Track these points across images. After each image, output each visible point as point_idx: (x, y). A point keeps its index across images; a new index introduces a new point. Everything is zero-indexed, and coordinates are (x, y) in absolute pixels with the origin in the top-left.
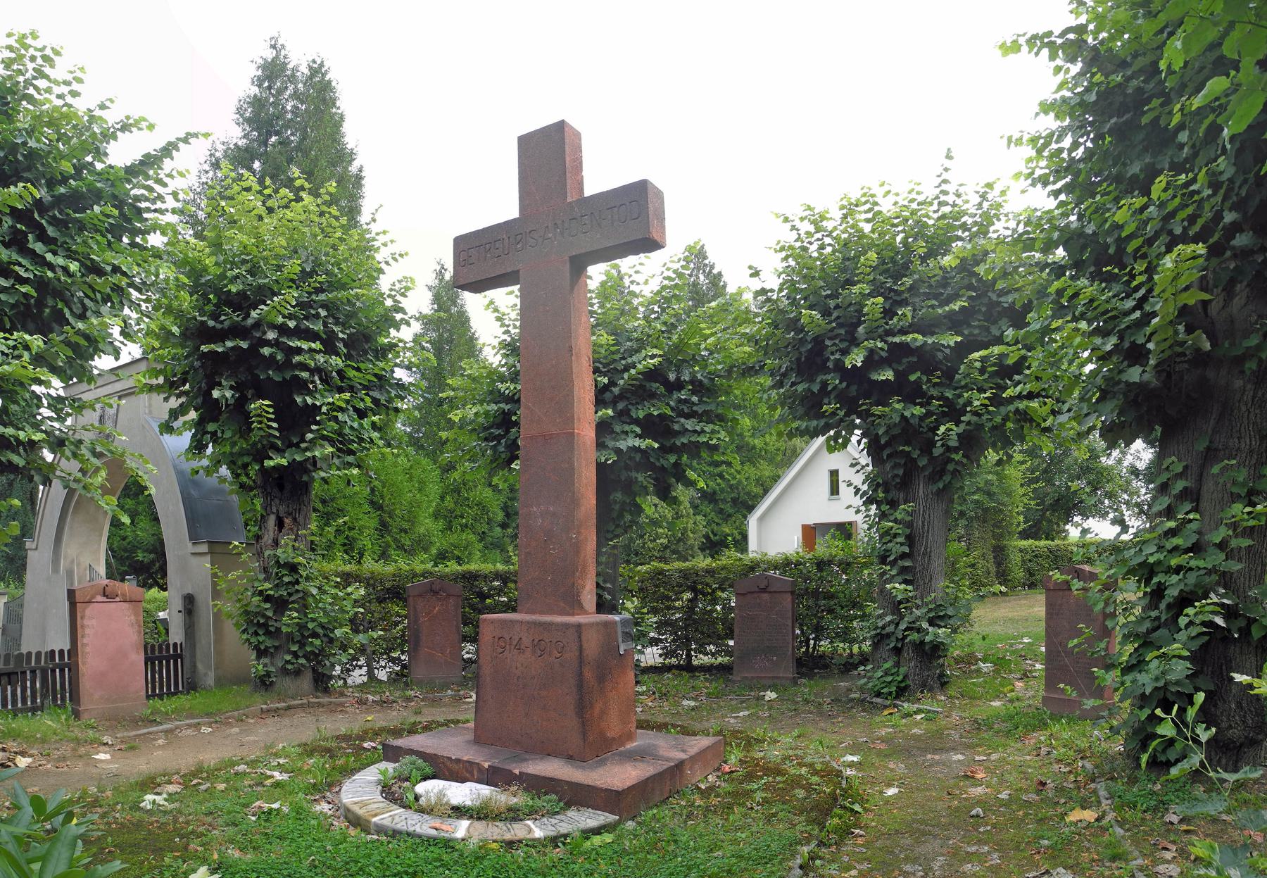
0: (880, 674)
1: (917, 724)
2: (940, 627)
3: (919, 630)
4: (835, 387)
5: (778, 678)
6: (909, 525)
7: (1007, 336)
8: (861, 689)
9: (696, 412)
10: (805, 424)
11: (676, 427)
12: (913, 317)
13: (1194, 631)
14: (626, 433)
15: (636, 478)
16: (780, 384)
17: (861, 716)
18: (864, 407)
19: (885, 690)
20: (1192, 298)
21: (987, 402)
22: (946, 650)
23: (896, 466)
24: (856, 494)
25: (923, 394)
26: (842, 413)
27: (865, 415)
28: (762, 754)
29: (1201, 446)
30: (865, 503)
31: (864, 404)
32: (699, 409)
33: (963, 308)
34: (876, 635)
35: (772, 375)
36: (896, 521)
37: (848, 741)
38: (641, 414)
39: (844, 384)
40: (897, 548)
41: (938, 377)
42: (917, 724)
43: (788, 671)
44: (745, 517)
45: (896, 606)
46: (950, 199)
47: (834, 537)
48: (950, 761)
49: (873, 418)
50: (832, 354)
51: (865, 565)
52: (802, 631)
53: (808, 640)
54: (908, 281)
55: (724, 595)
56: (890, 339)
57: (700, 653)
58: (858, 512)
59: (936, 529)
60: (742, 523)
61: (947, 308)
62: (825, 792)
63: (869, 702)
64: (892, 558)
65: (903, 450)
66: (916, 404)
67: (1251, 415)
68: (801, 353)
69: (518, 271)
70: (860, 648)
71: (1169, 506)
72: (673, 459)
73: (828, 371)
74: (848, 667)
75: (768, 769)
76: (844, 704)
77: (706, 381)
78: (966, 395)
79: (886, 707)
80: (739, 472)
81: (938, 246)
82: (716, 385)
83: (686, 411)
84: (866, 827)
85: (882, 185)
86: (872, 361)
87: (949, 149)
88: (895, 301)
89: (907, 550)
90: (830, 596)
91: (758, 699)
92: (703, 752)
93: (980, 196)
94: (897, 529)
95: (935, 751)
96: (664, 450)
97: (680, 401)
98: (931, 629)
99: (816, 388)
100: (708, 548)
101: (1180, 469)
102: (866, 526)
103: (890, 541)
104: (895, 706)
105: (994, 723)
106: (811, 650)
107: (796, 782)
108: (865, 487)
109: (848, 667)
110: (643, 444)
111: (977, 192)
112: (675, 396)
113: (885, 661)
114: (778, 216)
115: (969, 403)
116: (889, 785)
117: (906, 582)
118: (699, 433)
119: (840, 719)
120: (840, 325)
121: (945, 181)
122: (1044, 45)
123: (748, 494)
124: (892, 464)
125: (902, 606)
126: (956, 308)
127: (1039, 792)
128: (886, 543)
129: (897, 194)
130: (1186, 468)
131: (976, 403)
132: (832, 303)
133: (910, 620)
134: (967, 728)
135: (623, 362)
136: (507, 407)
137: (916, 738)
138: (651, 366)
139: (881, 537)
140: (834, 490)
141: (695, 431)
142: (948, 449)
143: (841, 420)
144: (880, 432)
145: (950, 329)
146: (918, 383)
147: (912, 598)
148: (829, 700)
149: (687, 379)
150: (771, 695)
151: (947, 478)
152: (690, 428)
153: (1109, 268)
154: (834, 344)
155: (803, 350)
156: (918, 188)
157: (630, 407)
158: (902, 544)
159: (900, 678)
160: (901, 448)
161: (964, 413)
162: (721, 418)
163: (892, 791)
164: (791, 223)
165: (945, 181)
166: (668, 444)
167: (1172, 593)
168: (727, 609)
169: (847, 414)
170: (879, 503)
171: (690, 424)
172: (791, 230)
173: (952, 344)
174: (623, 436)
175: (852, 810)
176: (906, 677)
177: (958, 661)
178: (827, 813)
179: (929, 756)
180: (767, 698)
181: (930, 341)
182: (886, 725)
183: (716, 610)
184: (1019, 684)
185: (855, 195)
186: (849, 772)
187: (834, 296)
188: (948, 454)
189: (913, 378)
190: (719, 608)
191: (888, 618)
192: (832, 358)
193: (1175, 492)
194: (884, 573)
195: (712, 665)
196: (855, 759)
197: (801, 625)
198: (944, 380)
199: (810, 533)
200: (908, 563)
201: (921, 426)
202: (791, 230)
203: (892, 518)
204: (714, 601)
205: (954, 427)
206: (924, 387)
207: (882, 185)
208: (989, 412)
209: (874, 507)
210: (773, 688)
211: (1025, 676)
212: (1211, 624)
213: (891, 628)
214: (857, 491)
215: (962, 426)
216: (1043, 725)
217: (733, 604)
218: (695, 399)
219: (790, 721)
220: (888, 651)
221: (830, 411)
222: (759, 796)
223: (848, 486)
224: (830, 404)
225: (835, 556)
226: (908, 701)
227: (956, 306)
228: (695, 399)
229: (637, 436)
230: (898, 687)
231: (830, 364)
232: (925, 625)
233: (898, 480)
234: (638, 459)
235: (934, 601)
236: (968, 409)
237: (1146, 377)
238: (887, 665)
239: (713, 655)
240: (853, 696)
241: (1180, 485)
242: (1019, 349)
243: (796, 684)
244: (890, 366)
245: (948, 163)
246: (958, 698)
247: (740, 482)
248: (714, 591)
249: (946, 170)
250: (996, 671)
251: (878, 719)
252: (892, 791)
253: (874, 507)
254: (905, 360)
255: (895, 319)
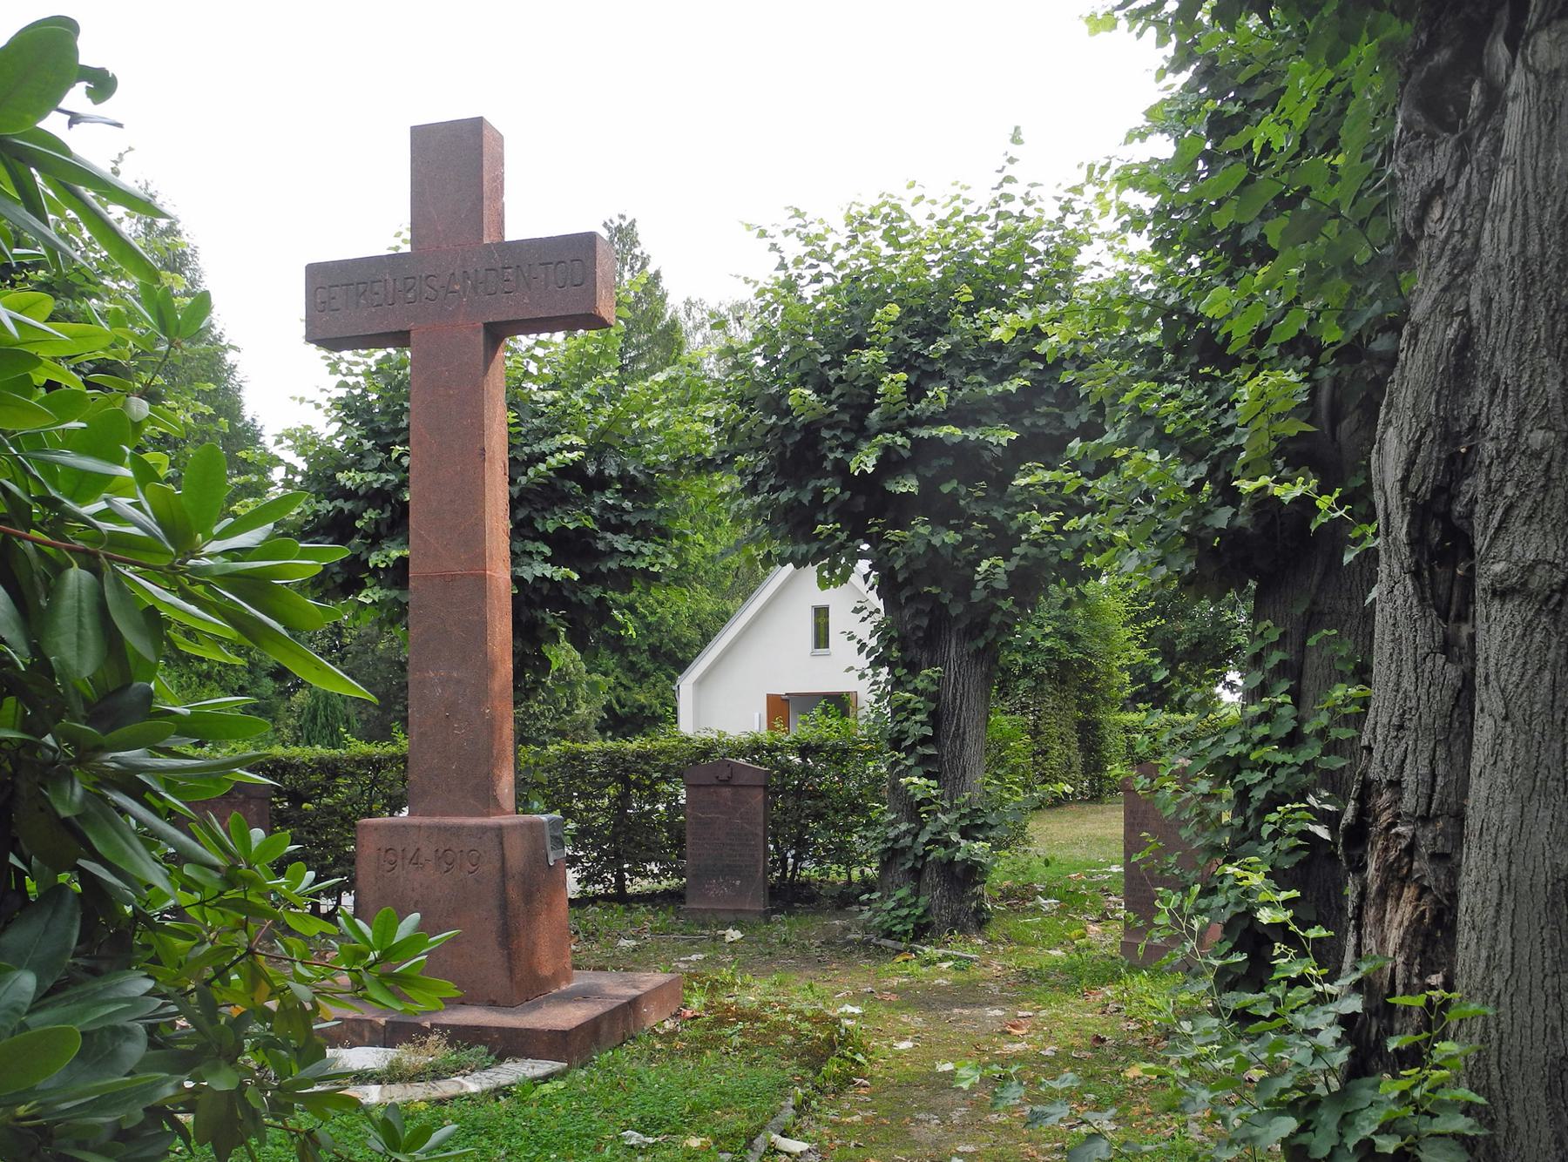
0: (891, 904)
1: (941, 973)
2: (976, 840)
3: (947, 844)
4: (835, 498)
5: (741, 911)
6: (935, 697)
7: (1072, 449)
8: (865, 928)
9: (628, 523)
10: (790, 549)
11: (601, 546)
12: (950, 398)
13: (1285, 844)
14: (530, 554)
15: (543, 619)
16: (752, 489)
17: (865, 964)
18: (876, 529)
19: (898, 928)
20: (1292, 428)
21: (1051, 528)
22: (985, 873)
23: (918, 614)
24: (860, 651)
25: (960, 513)
26: (842, 536)
27: (875, 540)
28: (732, 1000)
29: (1299, 610)
30: (872, 665)
31: (874, 525)
32: (633, 520)
33: (1022, 389)
34: (885, 851)
35: (741, 473)
36: (915, 691)
37: (847, 990)
38: (551, 527)
39: (848, 494)
40: (917, 728)
41: (982, 490)
42: (941, 973)
43: (756, 903)
44: (673, 679)
45: (914, 809)
46: (1015, 207)
47: (825, 712)
48: (984, 1017)
49: (888, 545)
50: (831, 450)
51: (869, 755)
52: (776, 847)
53: (784, 860)
54: (943, 345)
55: (669, 789)
56: (915, 432)
57: (638, 874)
58: (862, 676)
59: (972, 701)
60: (666, 688)
61: (1000, 388)
62: (819, 1038)
63: (875, 945)
64: (908, 742)
65: (929, 592)
66: (950, 528)
67: (1365, 571)
68: (784, 446)
69: (408, 332)
70: (862, 872)
71: (1262, 682)
72: (596, 592)
73: (825, 474)
74: (845, 899)
75: (743, 1015)
76: (841, 949)
77: (641, 477)
78: (1021, 516)
79: (899, 952)
80: (661, 604)
81: (990, 295)
82: (654, 484)
83: (613, 521)
84: (870, 1078)
85: (912, 186)
86: (890, 463)
87: (1017, 129)
88: (924, 372)
89: (929, 732)
90: (816, 795)
91: (715, 939)
92: (659, 989)
93: (1061, 208)
94: (917, 702)
95: (964, 1005)
96: (587, 579)
97: (605, 507)
98: (963, 843)
99: (806, 498)
100: (609, 728)
101: (1276, 637)
102: (873, 698)
103: (907, 719)
104: (913, 951)
105: (1049, 975)
106: (789, 875)
107: (780, 1028)
108: (873, 642)
109: (845, 899)
110: (559, 573)
111: (1059, 199)
112: (597, 499)
113: (899, 887)
114: (749, 227)
115: (1026, 528)
116: (901, 1039)
117: (928, 775)
118: (634, 556)
119: (834, 966)
120: (843, 408)
121: (1009, 179)
122: (1150, 23)
123: (677, 640)
124: (912, 611)
125: (922, 809)
126: (1013, 388)
127: (1094, 1049)
128: (902, 722)
129: (934, 202)
130: (1283, 636)
131: (1035, 529)
132: (832, 374)
133: (934, 830)
134: (1012, 980)
135: (527, 450)
136: (348, 506)
137: (937, 988)
138: (568, 461)
139: (895, 712)
140: (821, 638)
141: (629, 553)
142: (995, 593)
143: (842, 546)
144: (897, 566)
145: (1002, 418)
146: (954, 495)
147: (936, 797)
148: (817, 943)
149: (614, 474)
150: (733, 935)
151: (990, 634)
152: (621, 548)
153: (1207, 370)
154: (835, 437)
155: (789, 441)
156: (965, 194)
157: (534, 514)
158: (923, 724)
159: (919, 912)
160: (926, 589)
161: (1018, 543)
162: (664, 534)
163: (905, 1045)
164: (770, 240)
165: (1009, 179)
166: (588, 570)
167: (1259, 794)
168: (674, 809)
169: (851, 538)
170: (892, 666)
171: (621, 542)
172: (770, 250)
173: (1004, 442)
174: (526, 560)
175: (854, 1060)
176: (927, 911)
177: (1007, 895)
178: (824, 1059)
179: (956, 1011)
180: (728, 939)
181: (972, 437)
182: (900, 972)
183: (657, 811)
184: (1094, 929)
185: (869, 201)
186: (848, 1023)
187: (837, 363)
188: (992, 600)
189: (946, 489)
190: (661, 807)
191: (903, 827)
192: (831, 456)
193: (1269, 666)
194: (896, 763)
195: (654, 893)
196: (857, 1010)
197: (774, 836)
198: (992, 492)
199: (780, 707)
200: (930, 751)
201: (955, 558)
202: (770, 250)
203: (910, 687)
204: (655, 797)
205: (1001, 563)
206: (962, 503)
207: (912, 186)
208: (1055, 543)
209: (886, 670)
210: (737, 925)
211: (1104, 918)
212: (1305, 835)
213: (908, 840)
214: (862, 646)
215: (1015, 562)
216: (1116, 977)
217: (682, 802)
218: (627, 505)
219: (764, 968)
220: (904, 873)
221: (826, 533)
222: (737, 1041)
223: (849, 639)
224: (825, 522)
225: (827, 739)
226: (931, 943)
227: (1013, 385)
228: (627, 505)
229: (546, 560)
230: (916, 925)
231: (828, 465)
232: (955, 837)
233: (921, 634)
234: (545, 592)
235: (969, 803)
236: (1024, 537)
237: (1241, 521)
238: (901, 893)
239: (655, 876)
240: (851, 936)
241: (1276, 657)
242: (1077, 477)
243: (768, 922)
244: (914, 471)
245: (1015, 151)
246: (1003, 944)
247: (662, 619)
248: (654, 783)
249: (1011, 160)
250: (1062, 911)
251: (887, 967)
252: (905, 1045)
253: (886, 670)
254: (935, 463)
255: (923, 403)
